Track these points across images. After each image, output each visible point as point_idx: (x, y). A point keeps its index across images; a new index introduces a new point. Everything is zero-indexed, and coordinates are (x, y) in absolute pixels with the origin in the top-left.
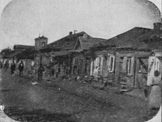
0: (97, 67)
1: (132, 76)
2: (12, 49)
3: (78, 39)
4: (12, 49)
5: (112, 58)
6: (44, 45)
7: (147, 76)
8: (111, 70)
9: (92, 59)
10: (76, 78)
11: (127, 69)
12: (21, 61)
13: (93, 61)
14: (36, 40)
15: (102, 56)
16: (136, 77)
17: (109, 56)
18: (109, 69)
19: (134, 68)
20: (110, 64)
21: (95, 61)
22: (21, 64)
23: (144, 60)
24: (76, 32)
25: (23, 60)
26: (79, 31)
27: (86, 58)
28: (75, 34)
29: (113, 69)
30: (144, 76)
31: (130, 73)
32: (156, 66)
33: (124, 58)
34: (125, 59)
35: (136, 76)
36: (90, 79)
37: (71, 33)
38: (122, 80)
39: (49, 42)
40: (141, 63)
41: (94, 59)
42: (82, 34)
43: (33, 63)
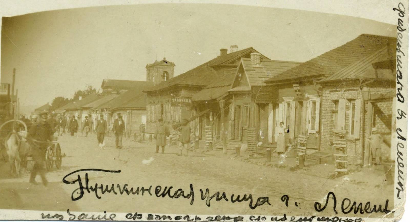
1: (357, 140)
2: (99, 89)
4: (99, 89)
5: (314, 103)
7: (390, 139)
8: (313, 128)
9: (271, 106)
10: (238, 149)
14: (149, 68)
15: (294, 100)
16: (367, 140)
17: (308, 99)
18: (309, 126)
19: (362, 122)
21: (277, 110)
22: (116, 121)
23: (382, 106)
26: (243, 46)
27: (362, 90)
30: (382, 140)
31: (352, 133)
33: (340, 101)
34: (343, 103)
35: (278, 135)
36: (268, 149)
37: (224, 51)
38: (338, 149)
39: (177, 72)
40: (378, 112)
41: (276, 106)
42: (247, 54)
43: (144, 119)
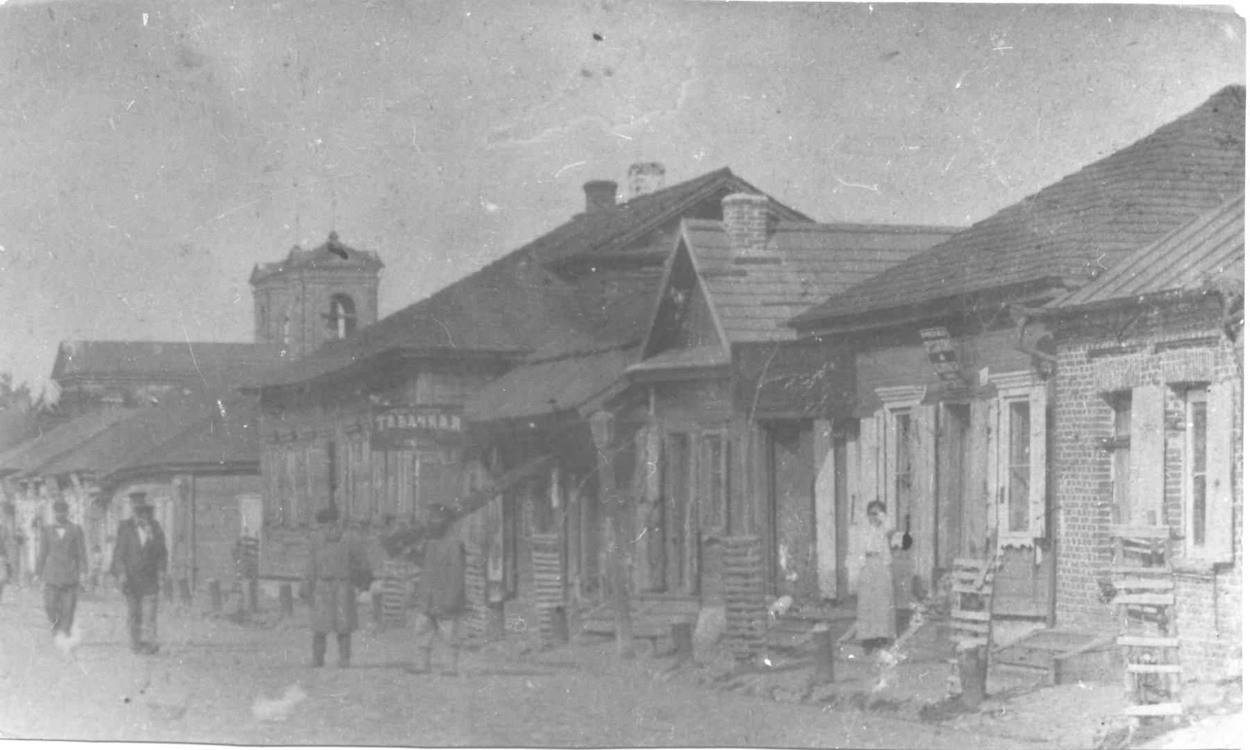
0: (877, 506)
3: (678, 239)
6: (350, 324)
8: (1019, 523)
9: (824, 430)
10: (683, 633)
11: (1170, 500)
12: (138, 497)
13: (838, 443)
14: (263, 280)
18: (1001, 515)
20: (1159, 581)
21: (851, 446)
24: (652, 184)
25: (149, 487)
28: (640, 204)
29: (1036, 511)
32: (1144, 263)
33: (1137, 394)
38: (1136, 615)
41: (847, 428)
